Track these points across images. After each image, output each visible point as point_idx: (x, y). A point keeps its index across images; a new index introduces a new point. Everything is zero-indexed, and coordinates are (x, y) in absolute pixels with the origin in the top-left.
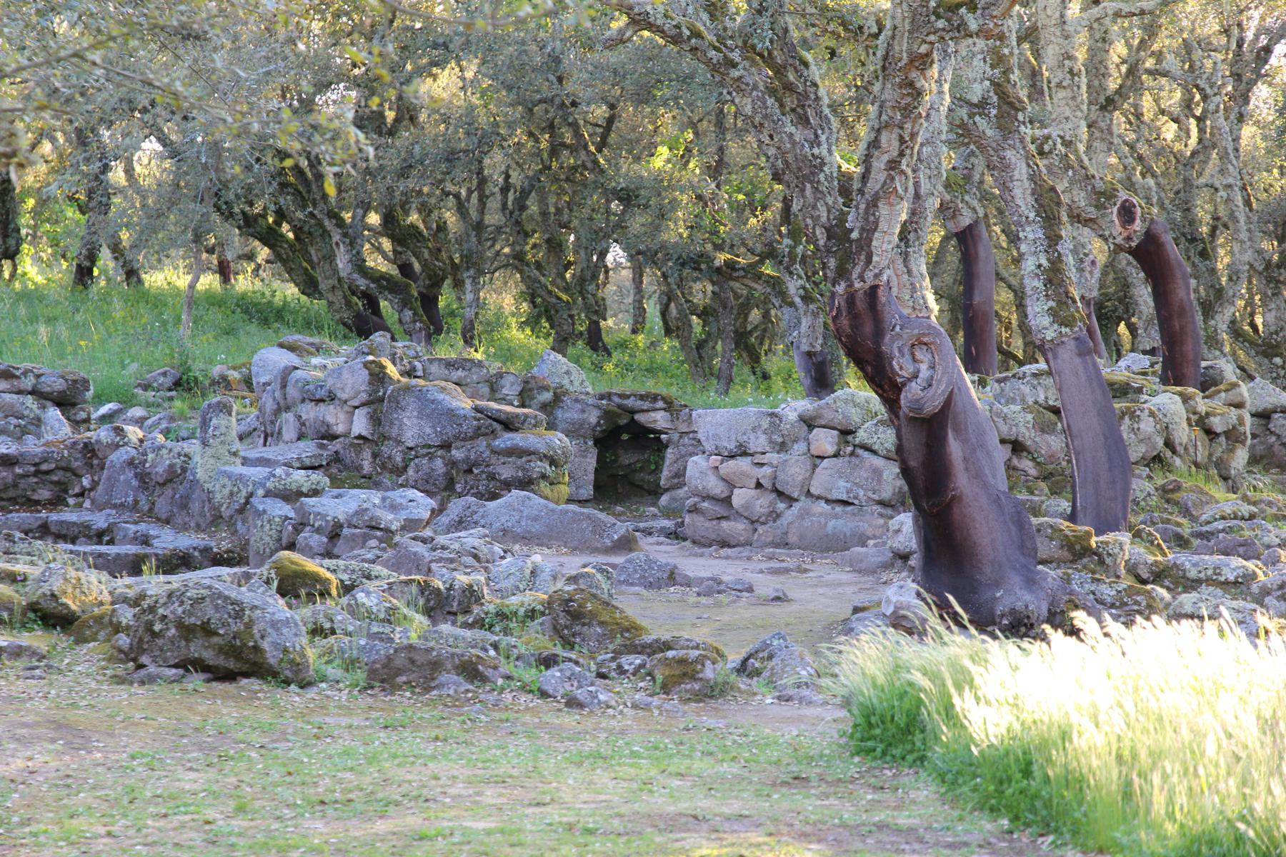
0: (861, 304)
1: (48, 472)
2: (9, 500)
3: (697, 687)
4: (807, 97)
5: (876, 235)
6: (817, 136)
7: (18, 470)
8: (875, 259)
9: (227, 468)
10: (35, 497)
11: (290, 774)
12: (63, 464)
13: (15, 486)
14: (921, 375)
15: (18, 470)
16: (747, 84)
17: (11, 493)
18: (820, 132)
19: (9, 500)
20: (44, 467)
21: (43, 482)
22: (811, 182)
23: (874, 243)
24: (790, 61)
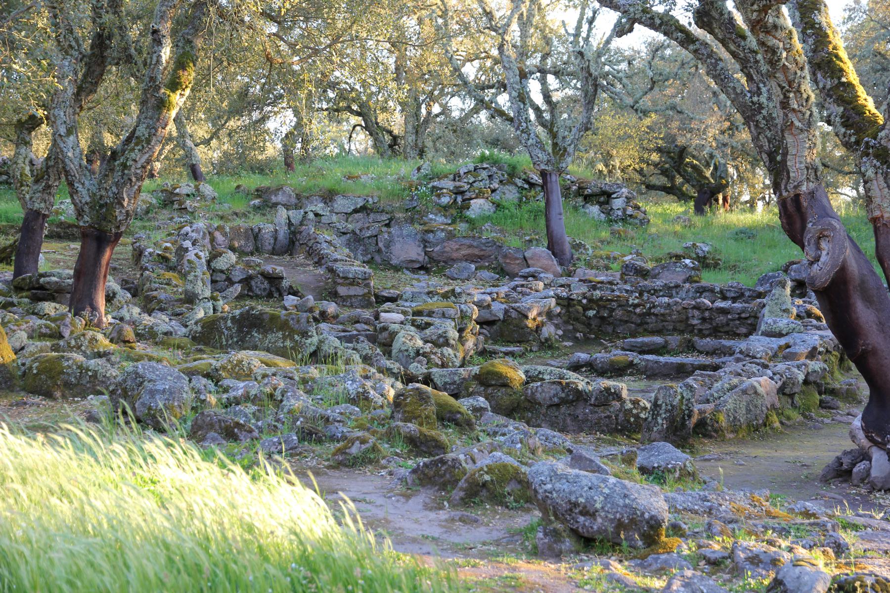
0: (791, 207)
1: (746, 318)
2: (725, 332)
3: (341, 458)
4: (749, 61)
5: (789, 157)
6: (759, 88)
7: (730, 317)
8: (792, 175)
9: (513, 305)
10: (738, 332)
11: (117, 487)
12: (752, 314)
13: (728, 325)
14: (822, 259)
15: (730, 317)
16: (703, 54)
17: (726, 329)
18: (761, 85)
19: (725, 332)
20: (743, 315)
21: (743, 324)
22: (753, 121)
23: (789, 163)
24: (728, 36)
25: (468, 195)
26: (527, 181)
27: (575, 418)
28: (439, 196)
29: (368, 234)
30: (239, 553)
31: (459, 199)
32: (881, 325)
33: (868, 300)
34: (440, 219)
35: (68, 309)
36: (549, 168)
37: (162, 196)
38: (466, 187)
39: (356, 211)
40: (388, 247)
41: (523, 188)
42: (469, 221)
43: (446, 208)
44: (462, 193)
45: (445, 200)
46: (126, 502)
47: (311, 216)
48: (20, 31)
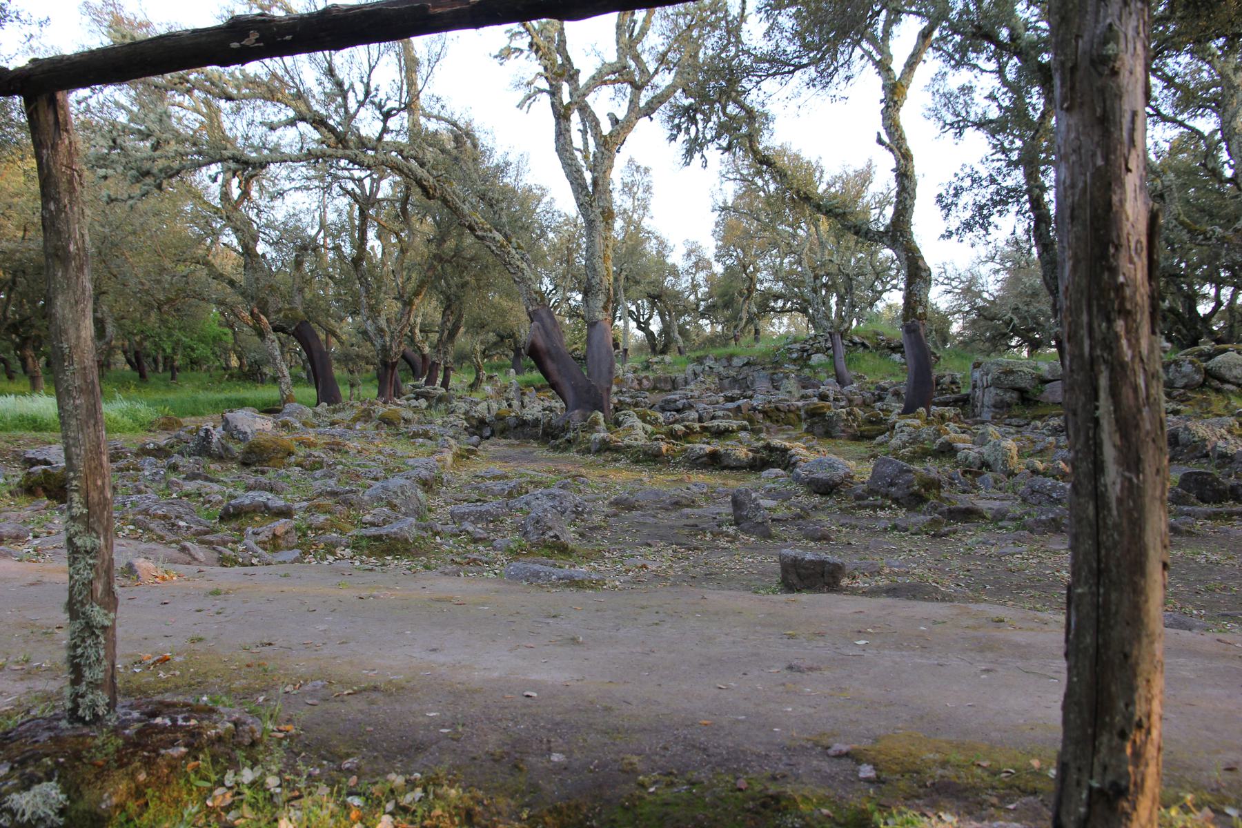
25: (810, 352)
26: (851, 341)
27: (523, 432)
28: (791, 353)
29: (741, 377)
30: (168, 425)
31: (805, 354)
32: (559, 371)
33: (552, 359)
34: (792, 367)
35: (376, 392)
36: (832, 331)
37: (645, 364)
38: (808, 347)
39: (744, 365)
40: (752, 384)
41: (848, 346)
42: (811, 367)
43: (795, 360)
44: (807, 351)
45: (795, 355)
46: (727, 542)
47: (707, 368)
48: (1172, 310)
